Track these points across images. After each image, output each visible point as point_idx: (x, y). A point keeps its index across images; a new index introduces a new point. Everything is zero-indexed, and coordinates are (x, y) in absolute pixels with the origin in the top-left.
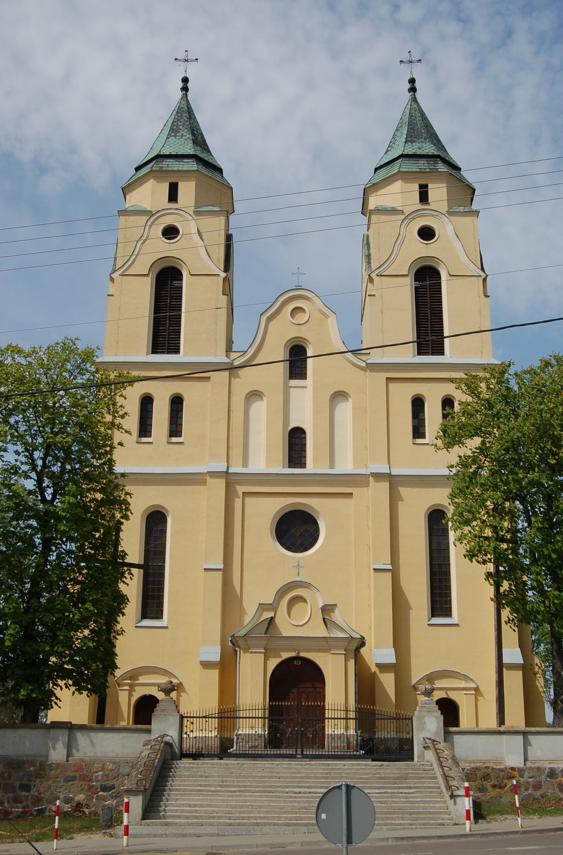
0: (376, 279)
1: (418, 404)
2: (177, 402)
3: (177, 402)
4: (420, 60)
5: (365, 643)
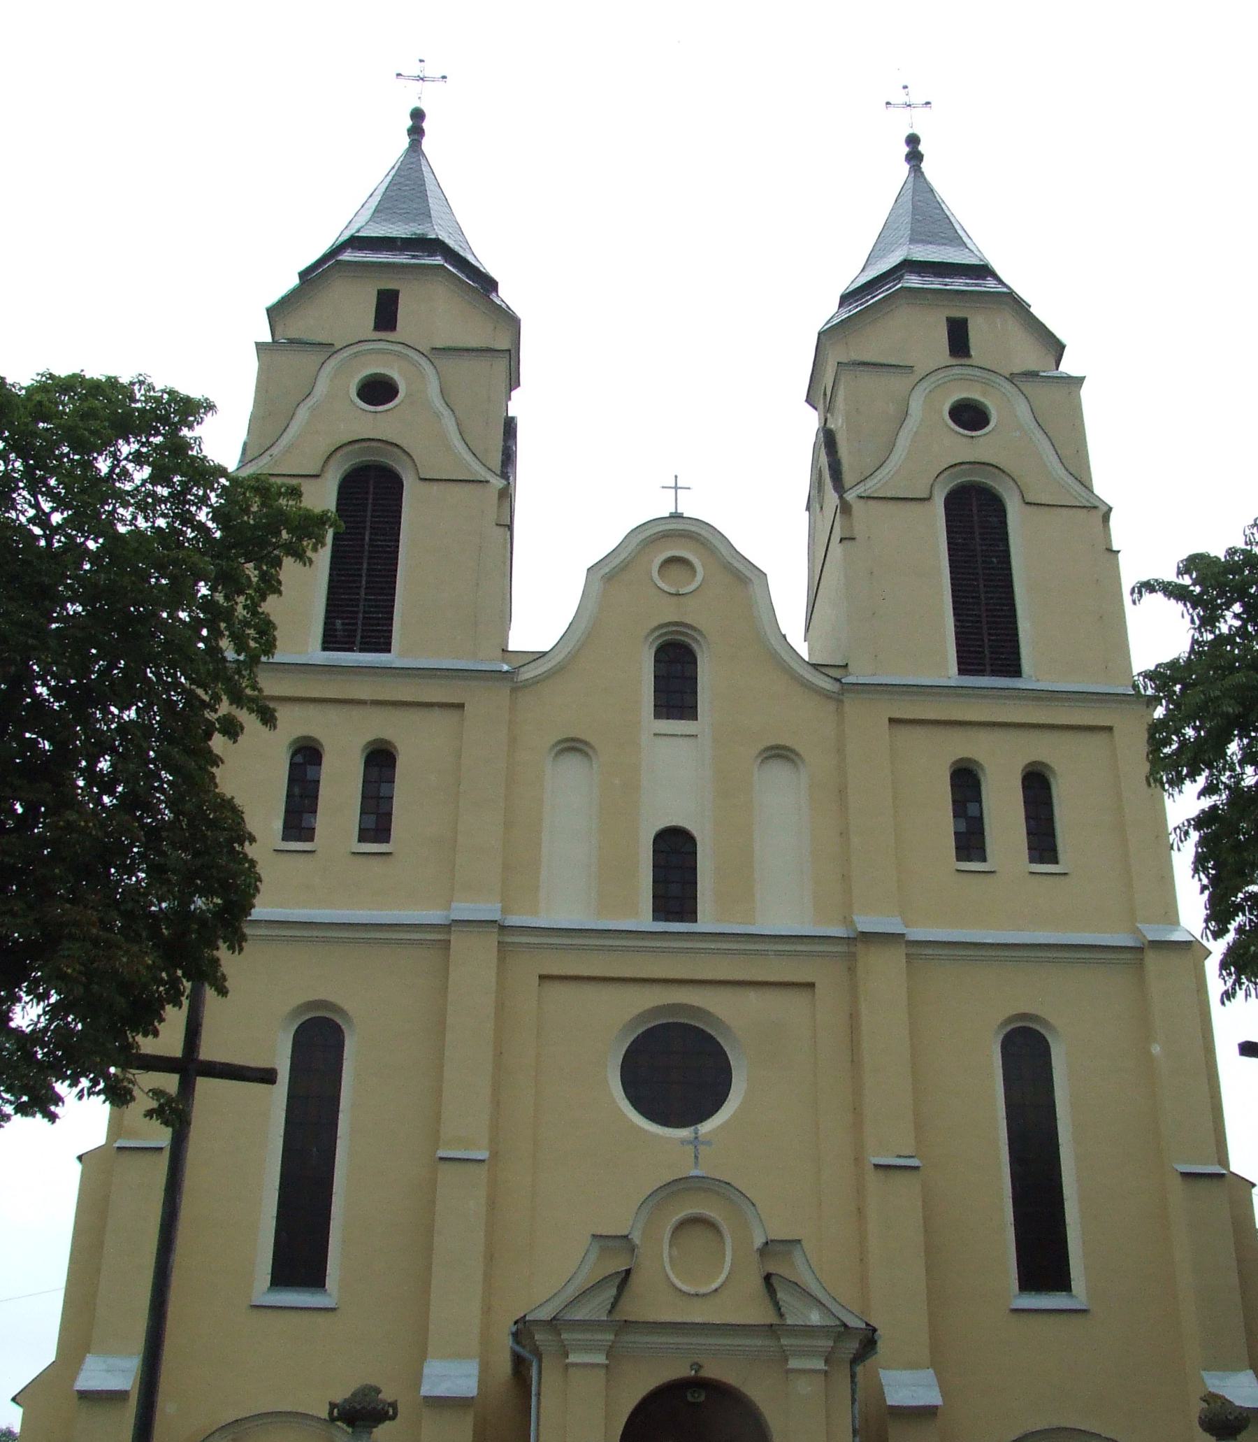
0: (858, 507)
1: (966, 781)
2: (380, 760)
3: (380, 760)
4: (928, 103)
5: (875, 1342)
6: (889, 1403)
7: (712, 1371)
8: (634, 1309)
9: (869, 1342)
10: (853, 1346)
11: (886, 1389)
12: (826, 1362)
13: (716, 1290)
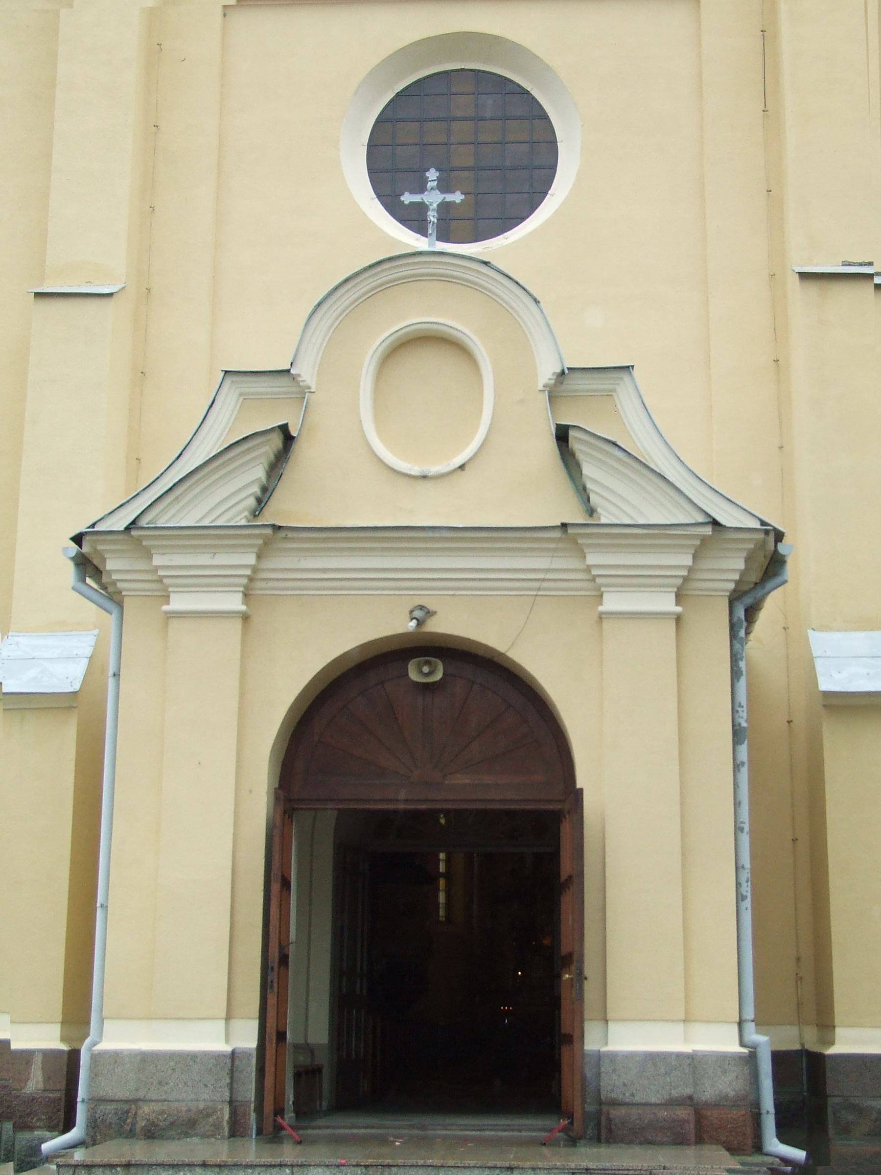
6: (825, 685)
7: (453, 622)
8: (301, 502)
9: (769, 563)
10: (731, 566)
11: (819, 665)
12: (679, 598)
13: (462, 467)
